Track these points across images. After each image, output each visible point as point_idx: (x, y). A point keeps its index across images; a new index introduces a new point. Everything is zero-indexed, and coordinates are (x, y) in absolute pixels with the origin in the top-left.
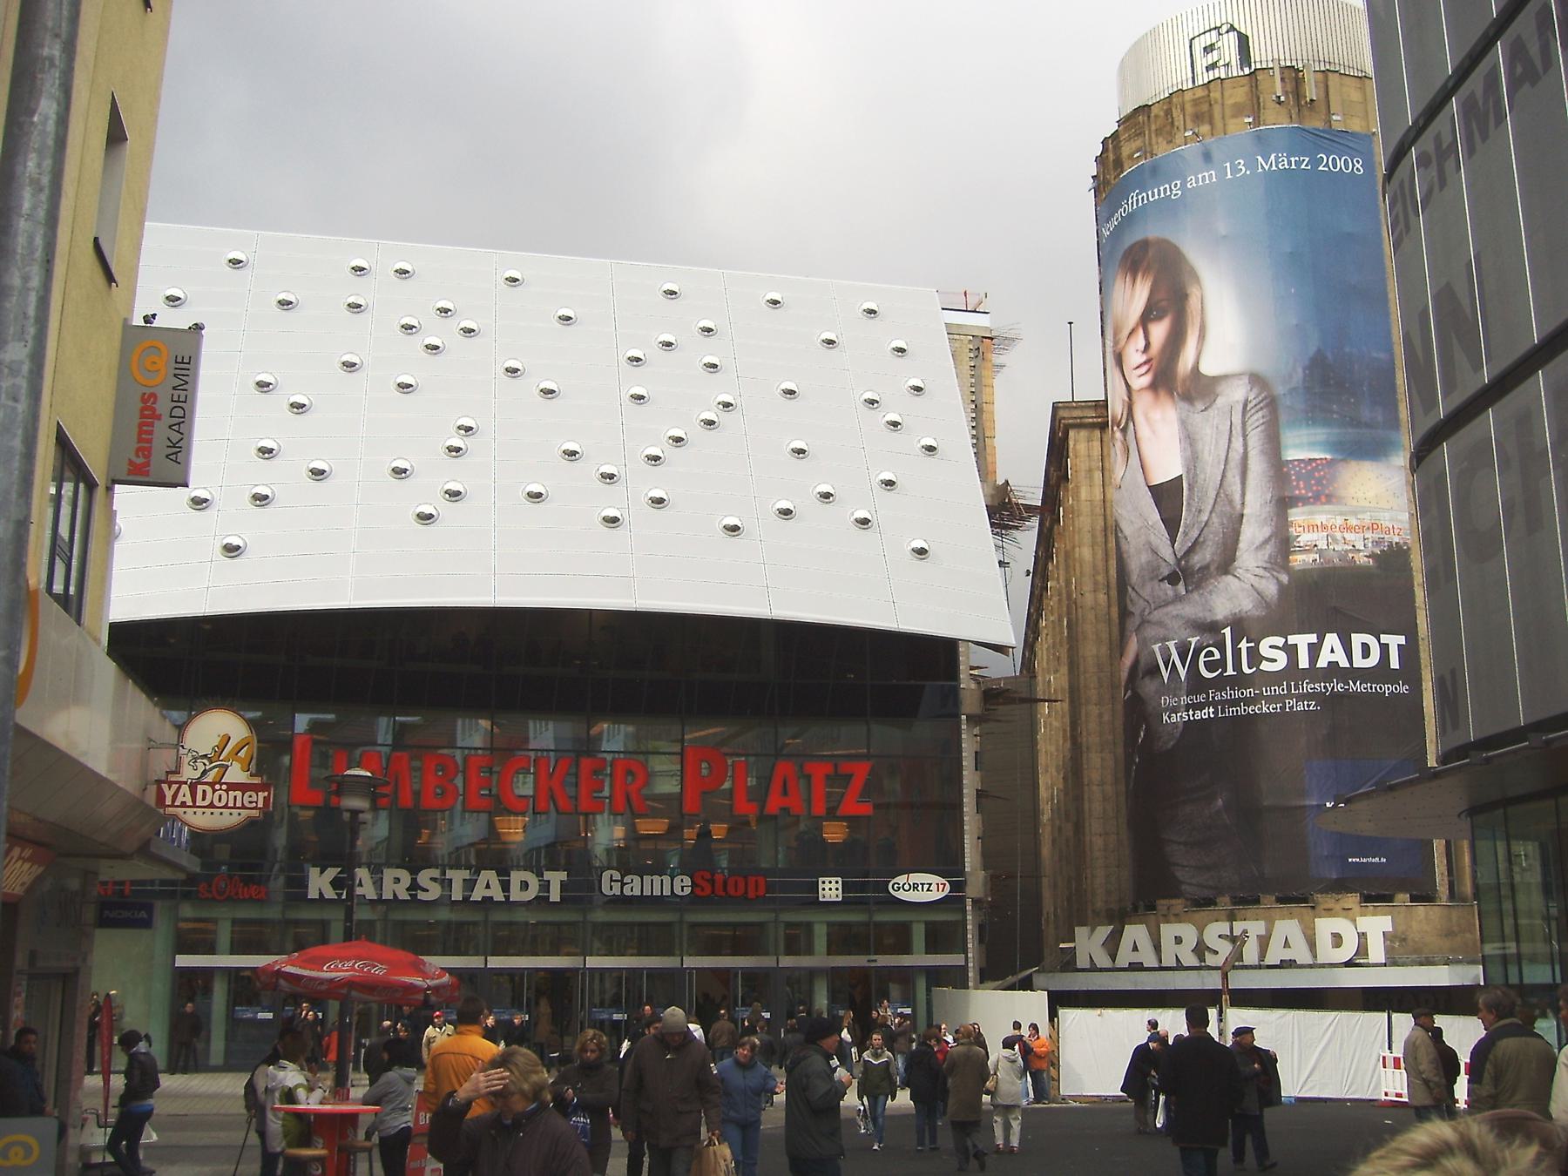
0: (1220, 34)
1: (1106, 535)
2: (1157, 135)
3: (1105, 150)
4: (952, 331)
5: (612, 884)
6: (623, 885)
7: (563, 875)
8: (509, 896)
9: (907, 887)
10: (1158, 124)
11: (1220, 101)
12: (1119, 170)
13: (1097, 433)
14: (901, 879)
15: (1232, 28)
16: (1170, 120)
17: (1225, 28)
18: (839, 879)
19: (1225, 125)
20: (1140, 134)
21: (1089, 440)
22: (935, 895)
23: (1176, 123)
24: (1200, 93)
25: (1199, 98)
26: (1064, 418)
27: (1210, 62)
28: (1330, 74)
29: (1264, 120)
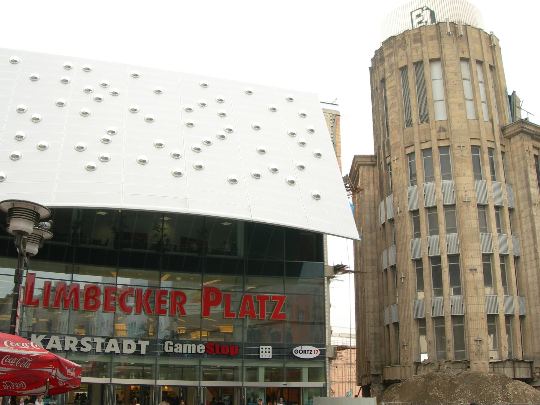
0: (423, 10)
1: (375, 210)
2: (398, 48)
3: (376, 55)
4: (325, 111)
5: (170, 347)
6: (174, 348)
7: (147, 343)
8: (64, 348)
9: (301, 352)
10: (399, 43)
11: (425, 34)
12: (383, 61)
13: (371, 167)
14: (299, 348)
15: (427, 8)
16: (404, 42)
17: (425, 8)
18: (271, 347)
19: (427, 43)
20: (392, 47)
21: (369, 170)
22: (313, 356)
23: (407, 43)
24: (416, 31)
25: (416, 33)
26: (358, 161)
27: (419, 21)
28: (467, 26)
29: (443, 42)
